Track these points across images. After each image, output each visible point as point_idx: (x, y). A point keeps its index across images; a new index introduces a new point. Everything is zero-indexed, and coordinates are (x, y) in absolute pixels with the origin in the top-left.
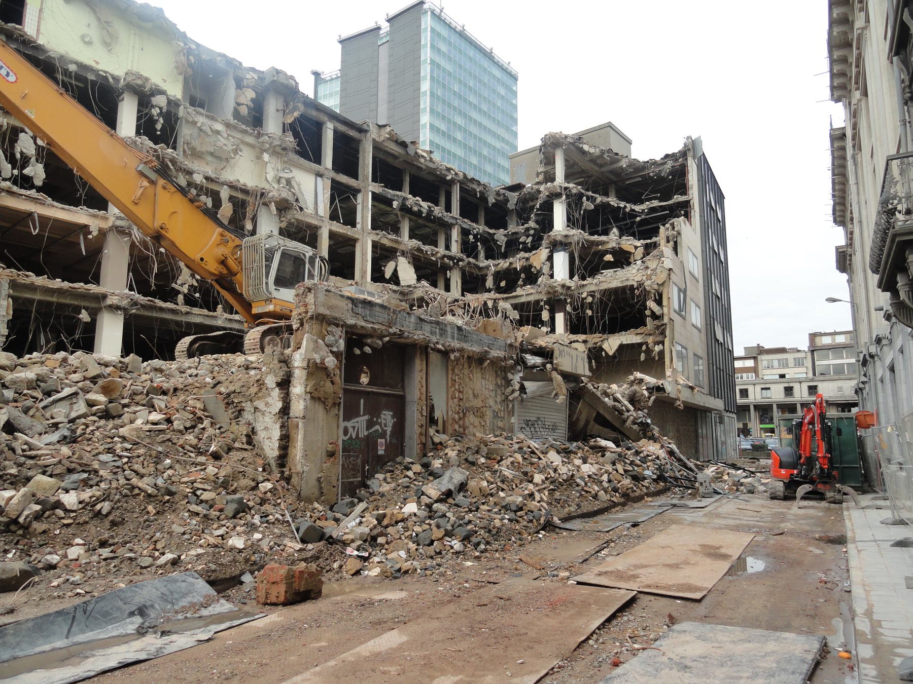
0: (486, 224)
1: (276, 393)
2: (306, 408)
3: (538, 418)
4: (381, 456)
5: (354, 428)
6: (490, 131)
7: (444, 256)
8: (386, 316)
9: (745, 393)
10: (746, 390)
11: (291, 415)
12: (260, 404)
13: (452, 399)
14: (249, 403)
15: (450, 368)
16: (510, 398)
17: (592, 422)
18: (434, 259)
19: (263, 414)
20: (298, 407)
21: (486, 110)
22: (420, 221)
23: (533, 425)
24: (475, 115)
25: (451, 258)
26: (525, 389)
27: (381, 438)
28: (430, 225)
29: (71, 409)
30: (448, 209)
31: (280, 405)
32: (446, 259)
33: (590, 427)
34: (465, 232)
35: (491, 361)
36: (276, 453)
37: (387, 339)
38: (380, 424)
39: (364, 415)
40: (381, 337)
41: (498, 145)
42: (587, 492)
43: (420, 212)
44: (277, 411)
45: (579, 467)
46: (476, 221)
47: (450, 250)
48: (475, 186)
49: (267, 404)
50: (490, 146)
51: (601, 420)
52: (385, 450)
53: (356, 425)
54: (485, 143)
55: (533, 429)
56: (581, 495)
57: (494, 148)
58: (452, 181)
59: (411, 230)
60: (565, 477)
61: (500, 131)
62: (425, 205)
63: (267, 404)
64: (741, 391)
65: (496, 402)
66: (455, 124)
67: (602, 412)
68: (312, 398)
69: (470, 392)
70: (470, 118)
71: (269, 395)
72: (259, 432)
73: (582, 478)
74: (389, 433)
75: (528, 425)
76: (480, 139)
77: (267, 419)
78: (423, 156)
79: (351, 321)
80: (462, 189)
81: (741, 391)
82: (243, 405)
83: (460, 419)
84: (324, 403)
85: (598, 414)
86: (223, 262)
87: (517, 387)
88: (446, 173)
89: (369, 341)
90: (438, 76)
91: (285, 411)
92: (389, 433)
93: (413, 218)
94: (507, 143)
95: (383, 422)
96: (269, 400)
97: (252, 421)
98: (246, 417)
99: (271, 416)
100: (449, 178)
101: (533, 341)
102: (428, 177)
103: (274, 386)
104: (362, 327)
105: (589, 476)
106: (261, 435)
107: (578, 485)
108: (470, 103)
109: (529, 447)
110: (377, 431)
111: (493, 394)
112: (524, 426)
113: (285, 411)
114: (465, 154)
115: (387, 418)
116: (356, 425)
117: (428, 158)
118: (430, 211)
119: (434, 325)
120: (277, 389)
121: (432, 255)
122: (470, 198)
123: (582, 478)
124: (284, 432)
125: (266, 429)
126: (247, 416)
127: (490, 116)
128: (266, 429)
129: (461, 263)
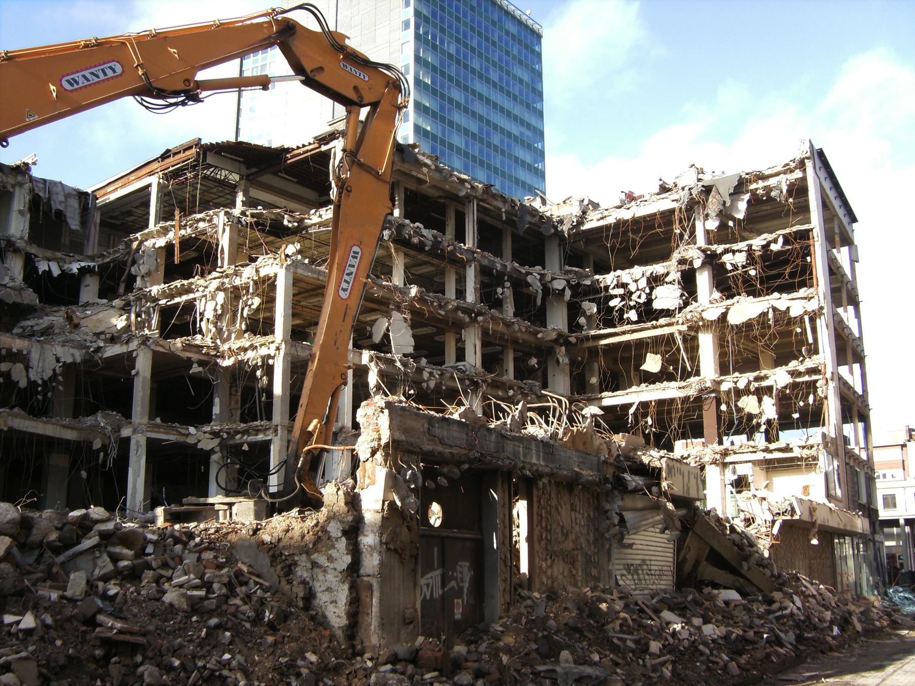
0: (516, 257)
1: (342, 544)
2: (382, 564)
3: (644, 560)
4: (459, 621)
5: (428, 585)
6: (502, 110)
7: (458, 308)
8: (464, 436)
9: (890, 501)
10: (893, 497)
11: (362, 572)
12: (321, 559)
13: (540, 541)
14: (304, 556)
15: (535, 499)
16: (607, 535)
17: (704, 563)
18: (442, 313)
19: (325, 571)
20: (371, 562)
21: (496, 80)
22: (422, 257)
23: (636, 570)
24: (480, 87)
25: (467, 311)
26: (625, 522)
27: (457, 598)
28: (435, 261)
29: (95, 566)
30: (460, 236)
31: (348, 559)
32: (460, 314)
33: (700, 569)
34: (484, 271)
35: (584, 487)
36: (344, 621)
37: (466, 466)
38: (456, 579)
39: (438, 568)
40: (458, 464)
41: (515, 129)
42: (714, 663)
43: (422, 244)
44: (345, 566)
45: (699, 628)
46: (498, 253)
47: (464, 298)
48: (499, 204)
49: (330, 559)
50: (502, 131)
51: (716, 559)
52: (462, 614)
53: (430, 581)
54: (495, 127)
55: (635, 577)
56: (708, 668)
57: (509, 134)
58: (468, 198)
59: (407, 268)
60: (686, 643)
61: (517, 110)
62: (428, 234)
63: (330, 559)
64: (885, 498)
65: (588, 541)
66: (451, 100)
67: (716, 547)
68: (388, 549)
69: (559, 530)
70: (474, 92)
71: (333, 547)
72: (319, 595)
73: (705, 644)
74: (465, 590)
75: (629, 572)
76: (488, 122)
77: (330, 577)
78: (426, 165)
79: (428, 447)
80: (481, 209)
81: (885, 498)
82: (296, 558)
83: (548, 567)
84: (400, 555)
85: (712, 550)
86: (630, 546)
87: (616, 520)
88: (460, 187)
89: (445, 470)
90: (426, 33)
91: (354, 568)
92: (465, 590)
93: (411, 252)
94: (528, 126)
95: (459, 575)
96: (333, 552)
97: (308, 579)
98: (299, 573)
99: (336, 573)
100: (463, 194)
101: (631, 454)
102: (434, 193)
103: (340, 535)
104: (440, 453)
105: (713, 641)
106: (322, 598)
107: (702, 654)
108: (473, 71)
109: (636, 604)
110: (453, 588)
111: (585, 531)
112: (625, 572)
113: (354, 568)
114: (467, 144)
115: (464, 572)
116: (430, 581)
117: (433, 167)
118: (436, 243)
119: (516, 443)
120: (344, 539)
121: (440, 307)
122: (488, 220)
123: (705, 644)
124: (354, 595)
125: (329, 590)
126: (302, 572)
127: (502, 89)
128: (329, 590)
129: (480, 318)
